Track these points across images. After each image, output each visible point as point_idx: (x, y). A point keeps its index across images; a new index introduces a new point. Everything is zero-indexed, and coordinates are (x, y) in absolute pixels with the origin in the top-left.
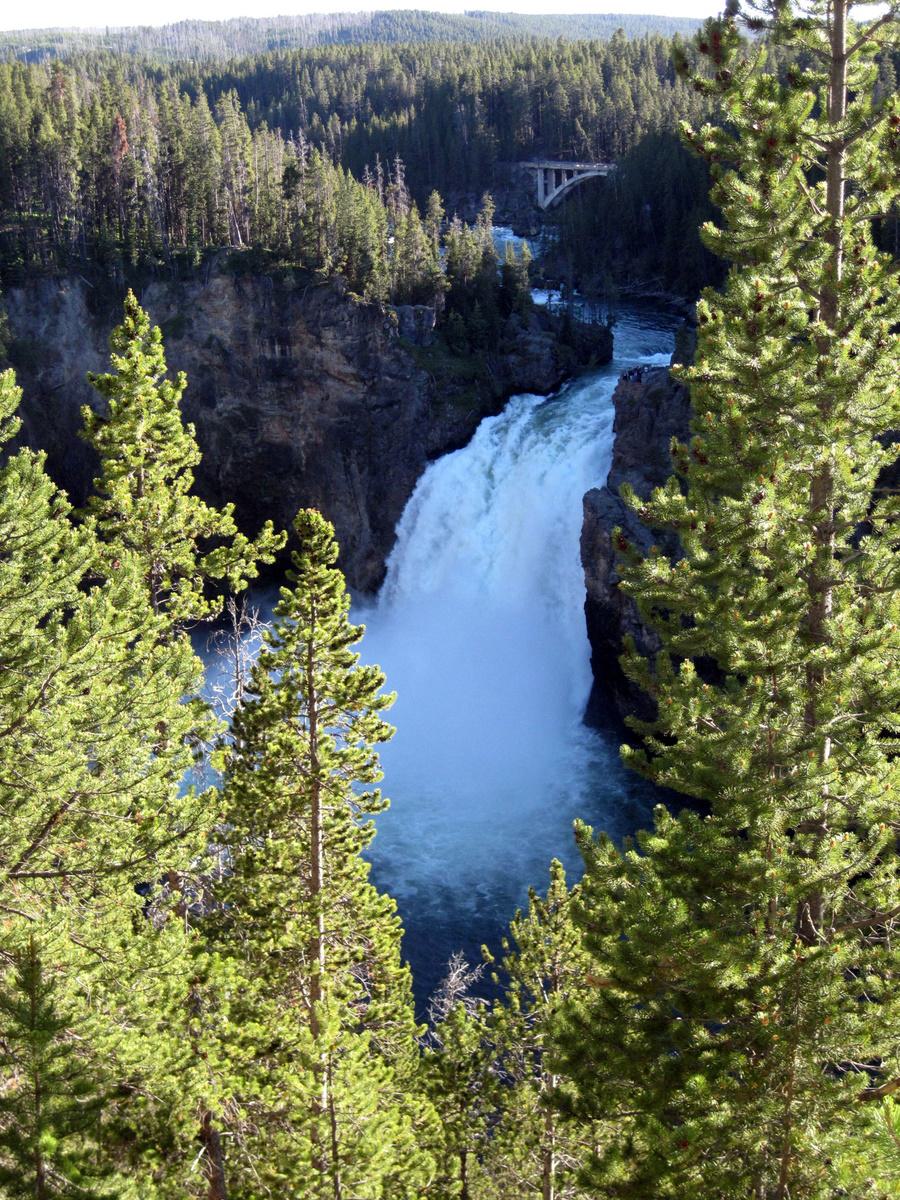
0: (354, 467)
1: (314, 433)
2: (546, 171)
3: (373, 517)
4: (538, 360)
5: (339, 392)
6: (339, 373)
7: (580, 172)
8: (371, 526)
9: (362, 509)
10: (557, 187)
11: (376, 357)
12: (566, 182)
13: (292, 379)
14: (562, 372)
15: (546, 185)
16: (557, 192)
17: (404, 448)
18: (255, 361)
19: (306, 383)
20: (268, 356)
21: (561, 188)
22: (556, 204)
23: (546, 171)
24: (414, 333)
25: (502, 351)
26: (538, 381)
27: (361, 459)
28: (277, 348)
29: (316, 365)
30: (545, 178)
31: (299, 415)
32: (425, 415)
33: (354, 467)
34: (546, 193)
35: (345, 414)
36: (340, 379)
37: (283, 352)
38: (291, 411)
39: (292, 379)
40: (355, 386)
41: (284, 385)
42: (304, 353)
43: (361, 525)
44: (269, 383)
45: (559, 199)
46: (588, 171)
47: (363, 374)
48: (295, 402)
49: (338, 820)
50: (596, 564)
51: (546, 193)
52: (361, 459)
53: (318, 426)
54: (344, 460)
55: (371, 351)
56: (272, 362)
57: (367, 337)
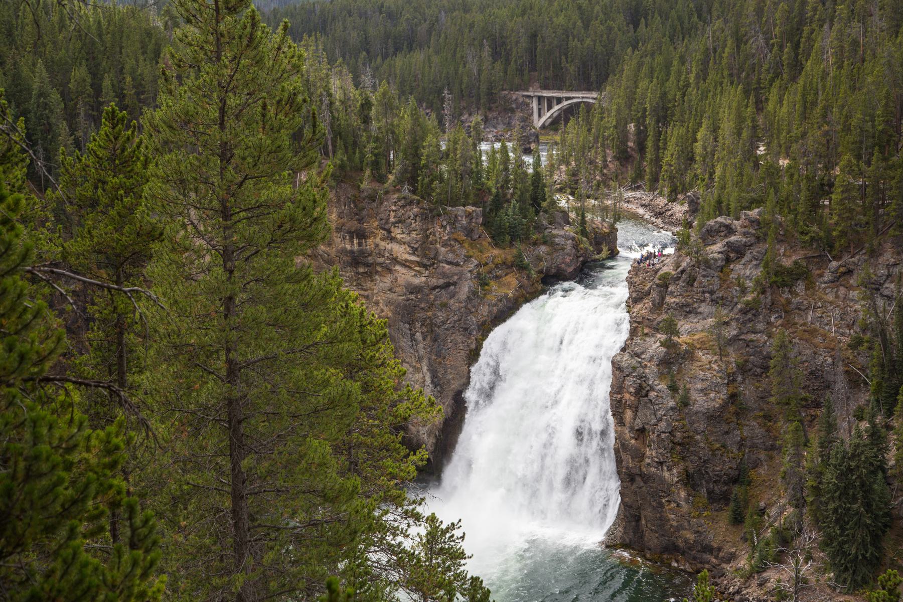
0: (419, 336)
1: (385, 309)
2: (540, 99)
3: (434, 375)
4: (563, 249)
5: (404, 276)
6: (406, 260)
7: (568, 99)
8: (432, 382)
9: (425, 369)
10: (548, 110)
11: (436, 249)
12: (556, 108)
13: (367, 265)
14: (581, 259)
15: (539, 110)
16: (548, 114)
17: (460, 320)
18: (338, 251)
19: (379, 269)
20: (348, 247)
21: (552, 111)
22: (547, 124)
23: (540, 99)
24: (466, 228)
25: (535, 244)
26: (563, 266)
27: (425, 329)
28: (356, 241)
29: (387, 254)
30: (539, 104)
31: (373, 294)
32: (475, 293)
33: (419, 336)
34: (540, 116)
35: (411, 293)
36: (405, 264)
37: (360, 244)
38: (366, 290)
39: (367, 265)
40: (418, 271)
41: (361, 270)
42: (377, 246)
43: (424, 381)
44: (348, 268)
45: (550, 120)
46: (574, 98)
47: (425, 261)
48: (369, 284)
49: (51, 579)
50: (623, 413)
51: (540, 116)
52: (425, 329)
53: (388, 303)
54: (410, 330)
55: (431, 243)
56: (352, 252)
57: (429, 232)
